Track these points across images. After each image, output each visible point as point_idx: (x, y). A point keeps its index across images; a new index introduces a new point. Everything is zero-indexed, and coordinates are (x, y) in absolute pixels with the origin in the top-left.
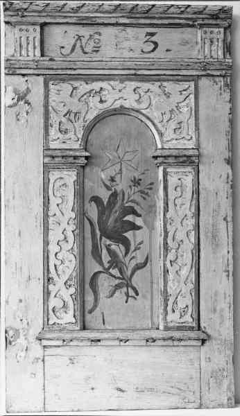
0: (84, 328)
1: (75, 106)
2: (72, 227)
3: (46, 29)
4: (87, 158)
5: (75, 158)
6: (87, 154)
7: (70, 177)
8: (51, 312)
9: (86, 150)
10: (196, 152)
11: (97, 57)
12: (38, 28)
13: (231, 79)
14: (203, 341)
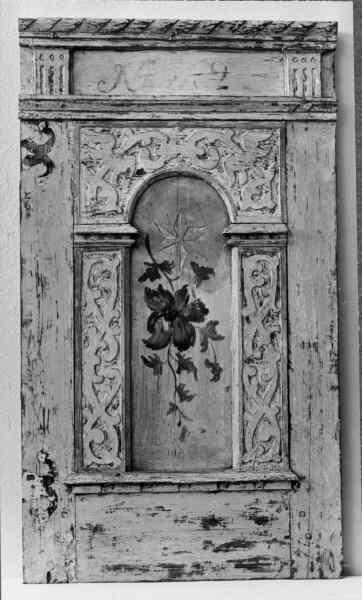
0: (131, 468)
4: (131, 236)
5: (118, 236)
6: (133, 230)
7: (113, 261)
8: (87, 450)
9: (132, 223)
10: (283, 228)
12: (66, 55)
13: (334, 57)
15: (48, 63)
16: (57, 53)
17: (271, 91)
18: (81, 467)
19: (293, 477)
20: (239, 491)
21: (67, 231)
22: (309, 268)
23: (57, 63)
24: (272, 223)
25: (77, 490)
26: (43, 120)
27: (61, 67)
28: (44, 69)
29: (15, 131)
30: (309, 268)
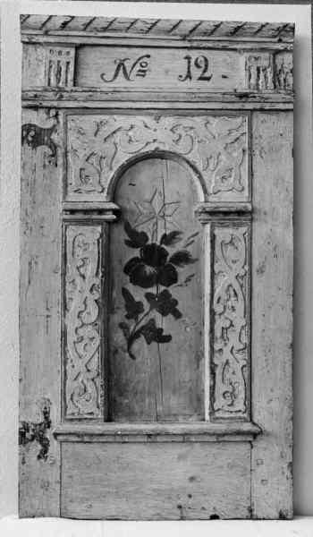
0: (109, 419)
1: (99, 147)
2: (97, 295)
3: (81, 52)
4: (115, 212)
5: (101, 212)
6: (113, 206)
7: (92, 234)
9: (114, 200)
11: (137, 83)
12: (73, 52)
14: (255, 435)
15: (55, 58)
16: (65, 50)
17: (170, 54)
18: (65, 417)
19: (255, 429)
20: (78, 442)
21: (61, 207)
22: (273, 230)
23: (64, 59)
24: (90, 161)
25: (60, 438)
26: (55, 108)
27: (68, 63)
28: (61, 64)
29: (15, 117)
30: (273, 230)
